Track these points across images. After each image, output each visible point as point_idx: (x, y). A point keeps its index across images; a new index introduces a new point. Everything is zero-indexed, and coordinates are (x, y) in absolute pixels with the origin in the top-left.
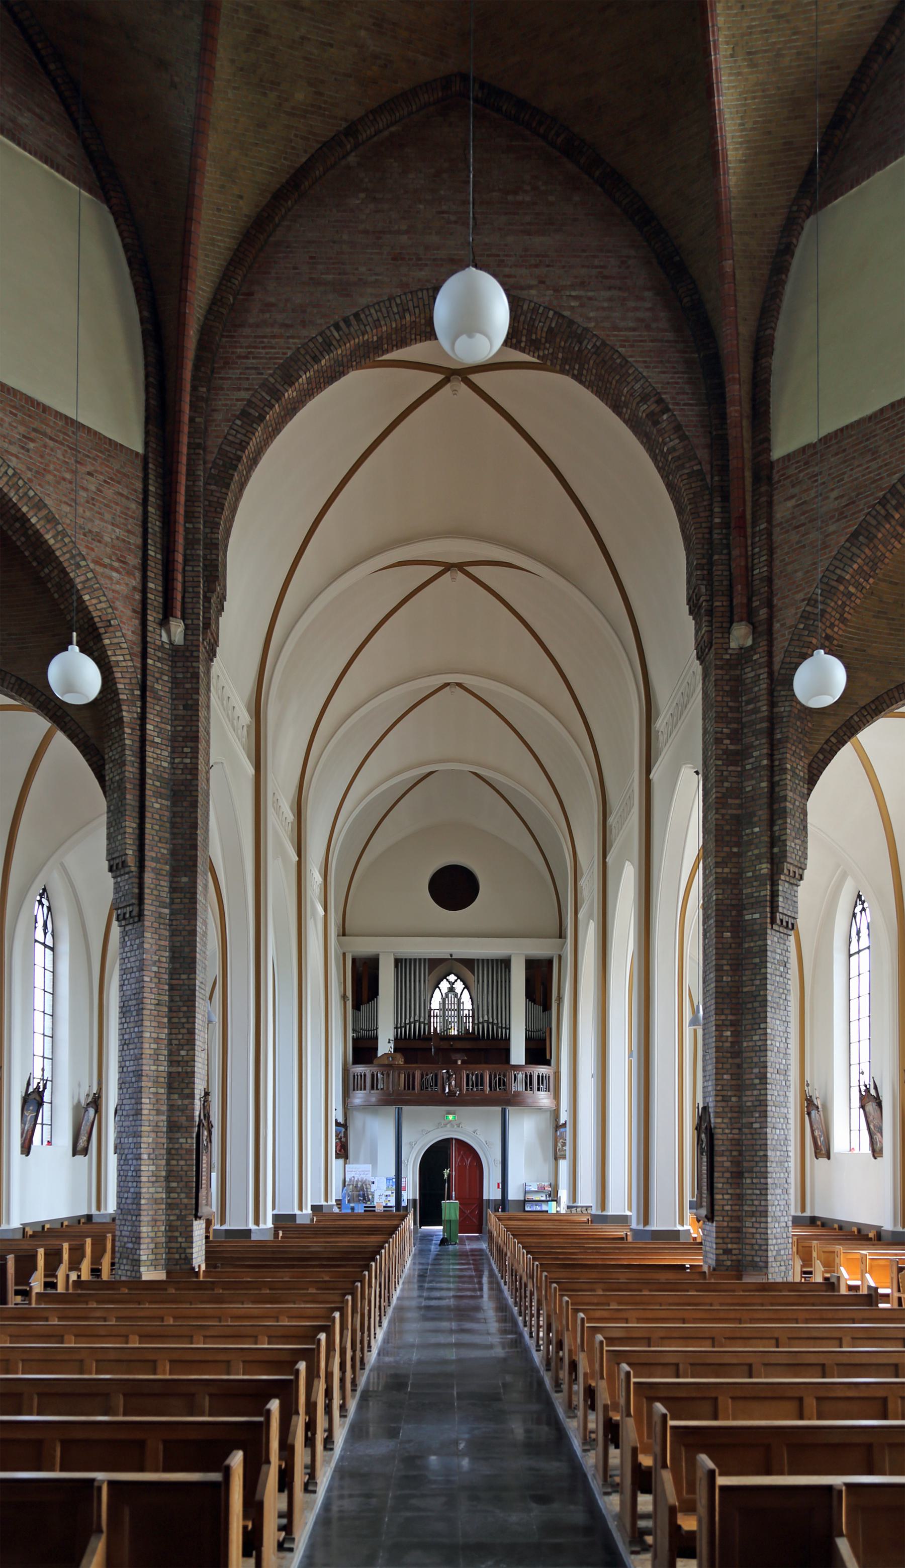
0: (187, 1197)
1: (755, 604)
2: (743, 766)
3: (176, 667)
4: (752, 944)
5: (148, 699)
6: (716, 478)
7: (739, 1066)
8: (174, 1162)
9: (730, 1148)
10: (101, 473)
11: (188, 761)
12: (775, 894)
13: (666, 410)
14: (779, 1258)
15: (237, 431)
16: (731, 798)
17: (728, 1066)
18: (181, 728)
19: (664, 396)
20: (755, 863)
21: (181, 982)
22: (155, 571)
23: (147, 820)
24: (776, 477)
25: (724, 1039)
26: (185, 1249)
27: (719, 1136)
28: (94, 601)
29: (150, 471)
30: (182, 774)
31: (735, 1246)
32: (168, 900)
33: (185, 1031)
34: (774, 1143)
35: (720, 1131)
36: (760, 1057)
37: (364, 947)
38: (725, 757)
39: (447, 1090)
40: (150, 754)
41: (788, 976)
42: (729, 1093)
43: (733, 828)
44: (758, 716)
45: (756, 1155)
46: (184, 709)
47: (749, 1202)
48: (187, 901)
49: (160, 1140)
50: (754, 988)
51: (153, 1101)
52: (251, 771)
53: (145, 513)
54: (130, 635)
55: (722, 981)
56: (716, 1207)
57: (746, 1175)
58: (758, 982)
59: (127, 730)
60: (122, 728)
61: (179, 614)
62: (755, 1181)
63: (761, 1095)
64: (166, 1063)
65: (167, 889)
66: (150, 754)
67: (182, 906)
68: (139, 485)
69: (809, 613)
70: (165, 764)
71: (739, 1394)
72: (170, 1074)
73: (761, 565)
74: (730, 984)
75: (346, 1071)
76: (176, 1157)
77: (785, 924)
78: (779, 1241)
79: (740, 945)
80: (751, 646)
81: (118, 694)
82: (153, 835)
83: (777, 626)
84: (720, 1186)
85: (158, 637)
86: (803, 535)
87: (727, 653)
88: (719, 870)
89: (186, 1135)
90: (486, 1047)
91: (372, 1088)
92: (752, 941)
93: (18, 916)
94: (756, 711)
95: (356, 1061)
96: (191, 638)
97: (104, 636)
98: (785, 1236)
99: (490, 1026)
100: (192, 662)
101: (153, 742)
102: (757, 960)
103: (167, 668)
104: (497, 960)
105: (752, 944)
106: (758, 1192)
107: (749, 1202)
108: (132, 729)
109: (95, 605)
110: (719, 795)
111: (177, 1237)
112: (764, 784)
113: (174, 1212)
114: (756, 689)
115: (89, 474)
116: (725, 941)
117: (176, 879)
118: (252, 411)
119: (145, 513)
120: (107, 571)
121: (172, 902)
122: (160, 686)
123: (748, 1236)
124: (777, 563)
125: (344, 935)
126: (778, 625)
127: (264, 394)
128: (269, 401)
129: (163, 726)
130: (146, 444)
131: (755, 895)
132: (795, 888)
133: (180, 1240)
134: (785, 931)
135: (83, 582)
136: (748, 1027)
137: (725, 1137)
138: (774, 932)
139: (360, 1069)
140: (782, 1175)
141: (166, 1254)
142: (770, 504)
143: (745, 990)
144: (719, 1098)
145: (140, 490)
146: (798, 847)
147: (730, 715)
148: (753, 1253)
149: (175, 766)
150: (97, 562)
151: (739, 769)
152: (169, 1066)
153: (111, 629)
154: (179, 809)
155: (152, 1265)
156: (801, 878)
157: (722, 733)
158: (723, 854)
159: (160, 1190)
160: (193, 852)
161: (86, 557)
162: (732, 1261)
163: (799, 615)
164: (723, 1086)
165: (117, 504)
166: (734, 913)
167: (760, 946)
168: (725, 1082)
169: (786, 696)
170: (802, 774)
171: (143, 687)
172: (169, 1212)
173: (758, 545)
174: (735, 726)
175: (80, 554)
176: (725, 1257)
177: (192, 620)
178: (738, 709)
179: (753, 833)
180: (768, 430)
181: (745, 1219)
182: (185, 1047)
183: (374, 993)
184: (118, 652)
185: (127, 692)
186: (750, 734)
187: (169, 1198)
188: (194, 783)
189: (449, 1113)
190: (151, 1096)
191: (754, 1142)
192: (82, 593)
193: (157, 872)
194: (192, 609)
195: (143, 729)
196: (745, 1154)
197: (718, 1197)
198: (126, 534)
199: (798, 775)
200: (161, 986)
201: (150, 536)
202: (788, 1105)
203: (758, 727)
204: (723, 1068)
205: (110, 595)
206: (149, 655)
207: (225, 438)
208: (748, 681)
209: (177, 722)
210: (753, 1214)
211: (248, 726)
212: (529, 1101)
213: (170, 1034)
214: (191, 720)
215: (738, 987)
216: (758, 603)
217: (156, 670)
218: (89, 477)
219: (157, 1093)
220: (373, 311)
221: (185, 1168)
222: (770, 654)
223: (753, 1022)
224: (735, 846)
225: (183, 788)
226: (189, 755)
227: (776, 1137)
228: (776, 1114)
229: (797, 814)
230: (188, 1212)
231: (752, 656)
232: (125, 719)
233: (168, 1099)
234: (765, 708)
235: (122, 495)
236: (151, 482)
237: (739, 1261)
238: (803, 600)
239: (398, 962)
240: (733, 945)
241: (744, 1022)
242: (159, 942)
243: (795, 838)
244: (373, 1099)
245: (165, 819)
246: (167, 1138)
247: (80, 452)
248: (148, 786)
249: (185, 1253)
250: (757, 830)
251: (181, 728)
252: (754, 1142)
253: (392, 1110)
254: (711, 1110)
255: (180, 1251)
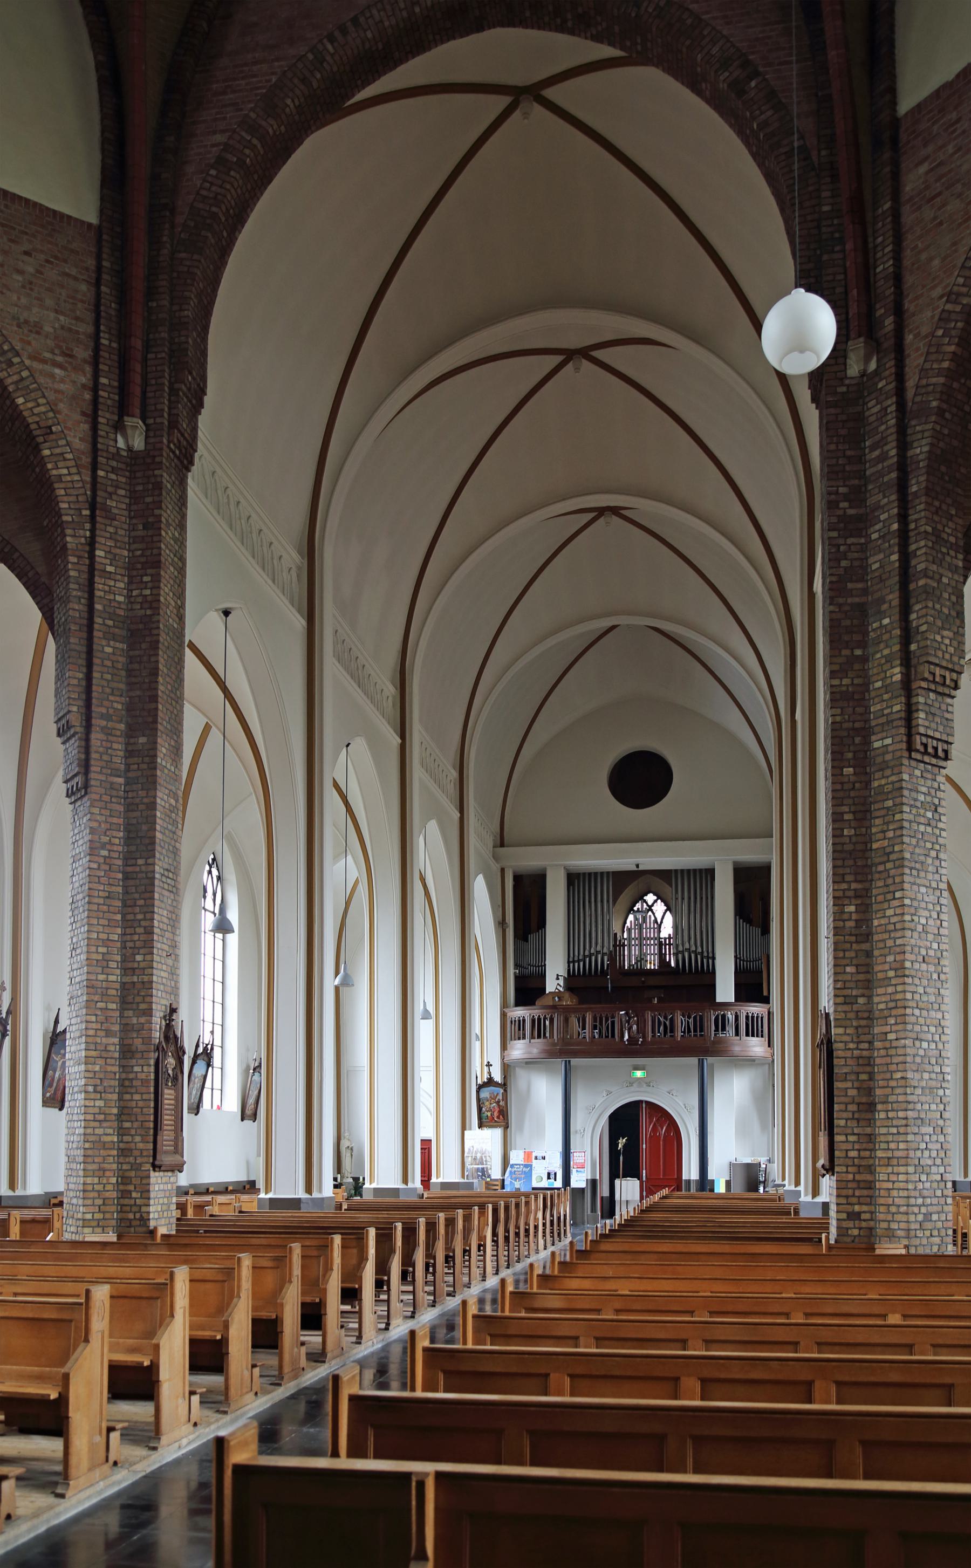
0: (142, 1141)
1: (891, 319)
2: (868, 536)
3: (135, 478)
4: (883, 782)
5: (98, 518)
6: (823, 153)
7: (869, 954)
8: (127, 1097)
9: (855, 1069)
10: (42, 251)
11: (148, 592)
12: (914, 708)
13: (756, 74)
14: (928, 1225)
15: (212, 184)
16: (851, 581)
17: (853, 954)
18: (139, 553)
19: (751, 57)
20: (885, 668)
21: (138, 869)
22: (109, 362)
23: (95, 668)
24: (903, 137)
25: (846, 916)
26: (140, 1206)
27: (841, 1054)
28: (30, 405)
29: (104, 243)
30: (141, 608)
31: (865, 1208)
32: (123, 767)
33: (141, 930)
34: (918, 1060)
35: (841, 1045)
36: (895, 939)
37: (528, 859)
38: (842, 525)
39: (626, 1037)
40: (100, 586)
41: (940, 825)
42: (854, 993)
43: (855, 622)
44: (885, 464)
45: (892, 1079)
46: (144, 528)
47: (883, 1146)
48: (145, 766)
49: (109, 1068)
50: (886, 843)
51: (101, 1018)
52: (300, 623)
53: (98, 295)
54: (77, 443)
55: (842, 835)
56: (837, 1153)
57: (879, 1107)
58: (891, 834)
59: (73, 559)
60: (66, 557)
61: (137, 411)
62: (891, 1115)
63: (896, 992)
64: (118, 972)
65: (121, 754)
66: (100, 586)
67: (139, 773)
68: (91, 262)
69: (950, 312)
70: (121, 599)
71: (579, 1370)
72: (123, 984)
73: (885, 259)
74: (854, 839)
75: (503, 1016)
76: (129, 1090)
77: (930, 750)
78: (928, 1201)
79: (867, 784)
80: (876, 370)
81: (61, 516)
82: (103, 687)
83: (909, 338)
84: (842, 1123)
85: (112, 443)
86: (939, 209)
87: (843, 385)
88: (836, 682)
89: (141, 1062)
90: (687, 982)
91: (532, 1037)
92: (883, 777)
93: (38, 816)
94: (883, 457)
95: (518, 1003)
96: (152, 440)
97: (42, 446)
98: (939, 1193)
99: (693, 956)
100: (153, 470)
101: (104, 571)
102: (890, 803)
103: (124, 480)
104: (701, 870)
105: (883, 782)
106: (894, 1130)
107: (883, 1146)
108: (79, 557)
109: (31, 409)
110: (834, 579)
111: (130, 1192)
112: (895, 557)
113: (127, 1160)
114: (883, 427)
115: (26, 253)
116: (846, 780)
117: (132, 740)
118: (229, 156)
119: (98, 295)
120: (47, 368)
121: (128, 770)
122: (117, 504)
123: (883, 1193)
124: (908, 253)
125: (502, 845)
126: (911, 336)
127: (243, 134)
128: (250, 141)
129: (118, 551)
130: (102, 212)
131: (886, 712)
132: (949, 700)
133: (134, 1195)
134: (934, 761)
135: (16, 383)
136: (880, 898)
137: (849, 1054)
138: (913, 763)
139: (520, 1012)
140: (933, 1107)
141: (118, 1212)
142: (896, 176)
143: (875, 846)
144: (840, 1000)
145: (93, 268)
146: (947, 641)
147: (848, 468)
148: (890, 1217)
149: (132, 600)
150: (32, 357)
151: (863, 541)
152: (122, 976)
153: (53, 437)
154: (137, 653)
155: (98, 1226)
156: (956, 687)
157: (837, 493)
158: (840, 660)
159: (111, 1131)
160: (153, 706)
161: (21, 352)
162: (860, 1229)
163: (937, 317)
164: (845, 982)
165: (62, 287)
166: (857, 740)
167: (893, 783)
168: (848, 977)
169: (923, 431)
170: (952, 539)
171: (93, 506)
172: (121, 1160)
173: (881, 232)
174: (856, 482)
175: (12, 348)
176: (851, 1224)
177: (155, 418)
178: (860, 459)
179: (881, 626)
180: (893, 77)
181: (878, 1169)
182: (142, 951)
183: (542, 924)
184: (60, 464)
185: (72, 512)
186: (877, 490)
187: (122, 1142)
188: (155, 618)
189: (637, 1068)
190: (99, 1013)
191: (888, 1060)
192: (14, 395)
193: (107, 732)
194: (155, 404)
195: (92, 556)
196: (877, 1077)
197: (838, 1138)
198: (74, 322)
199: (947, 541)
200: (113, 875)
201: (102, 321)
202: (943, 1007)
203: (886, 479)
204: (844, 957)
205: (51, 396)
206: (99, 466)
207: (198, 193)
208: (872, 419)
209: (134, 547)
210: (888, 1162)
211: (299, 568)
212: (737, 1049)
213: (124, 934)
214: (153, 542)
215: (866, 843)
216: (882, 311)
217: (110, 483)
218: (26, 258)
219: (106, 1009)
220: (375, 12)
221: (141, 1104)
222: (900, 377)
223: (886, 890)
224: (858, 648)
225: (141, 626)
226: (150, 585)
227: (921, 1052)
228: (921, 1021)
229: (946, 595)
230: (145, 1159)
231: (877, 384)
232: (69, 546)
233: (121, 1016)
234: (893, 452)
235: (68, 275)
236: (105, 256)
237: (871, 1229)
238: (941, 297)
239: (574, 879)
240: (857, 785)
241: (874, 892)
242: (110, 820)
243: (943, 628)
244: (535, 1051)
245: (120, 666)
246: (120, 1066)
247: (14, 229)
248: (96, 626)
249: (140, 1212)
250: (886, 621)
251: (139, 553)
252: (888, 1060)
253: (560, 1064)
254: (832, 1018)
255: (134, 1209)
